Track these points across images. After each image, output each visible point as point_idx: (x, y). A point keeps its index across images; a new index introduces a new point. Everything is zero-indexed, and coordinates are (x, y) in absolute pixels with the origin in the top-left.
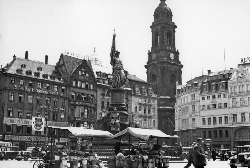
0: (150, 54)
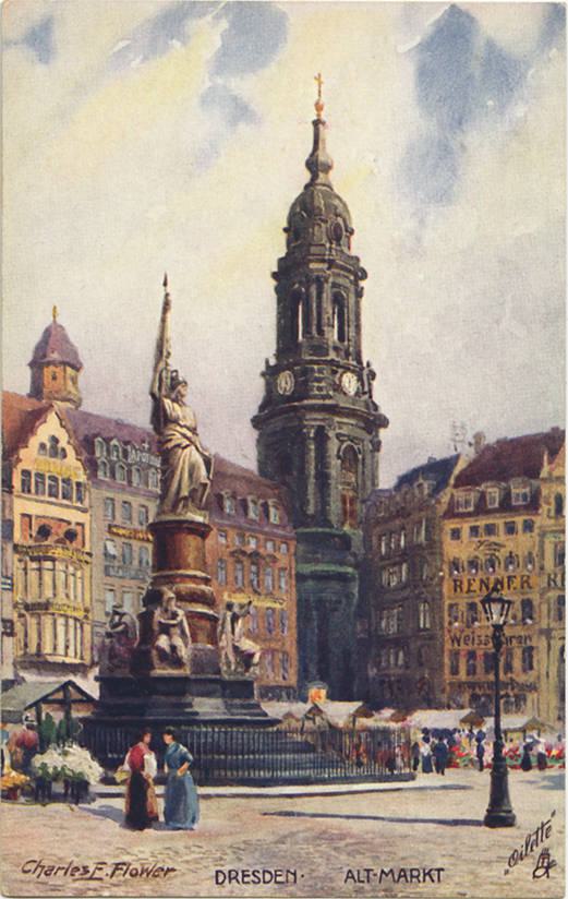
0: (271, 373)
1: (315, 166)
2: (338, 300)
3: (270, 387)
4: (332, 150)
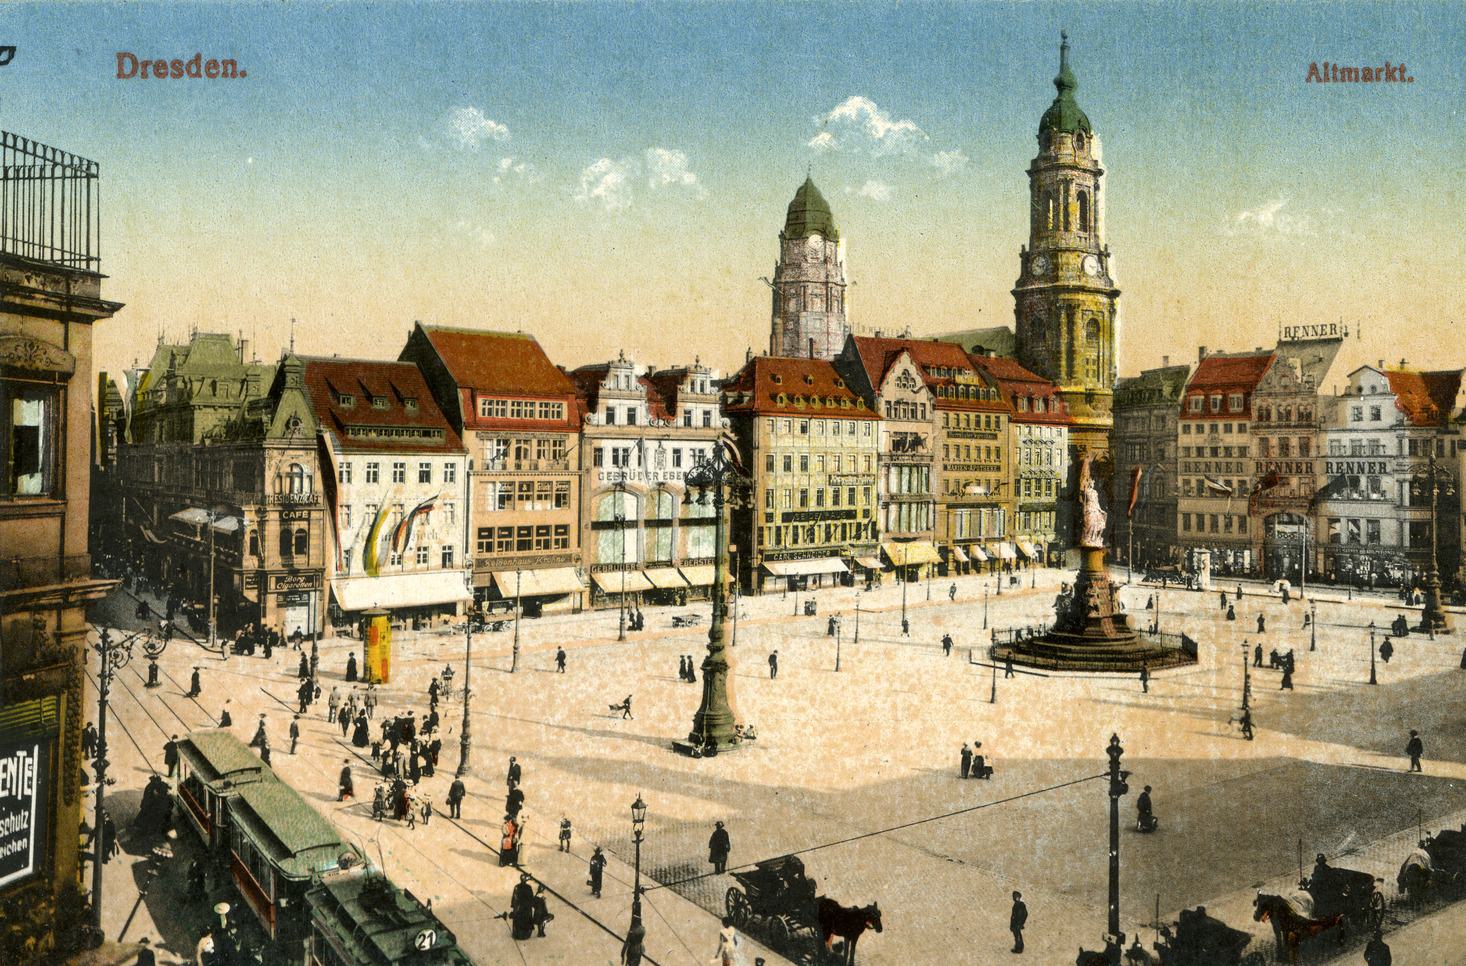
0: (1027, 258)
4: (1077, 72)
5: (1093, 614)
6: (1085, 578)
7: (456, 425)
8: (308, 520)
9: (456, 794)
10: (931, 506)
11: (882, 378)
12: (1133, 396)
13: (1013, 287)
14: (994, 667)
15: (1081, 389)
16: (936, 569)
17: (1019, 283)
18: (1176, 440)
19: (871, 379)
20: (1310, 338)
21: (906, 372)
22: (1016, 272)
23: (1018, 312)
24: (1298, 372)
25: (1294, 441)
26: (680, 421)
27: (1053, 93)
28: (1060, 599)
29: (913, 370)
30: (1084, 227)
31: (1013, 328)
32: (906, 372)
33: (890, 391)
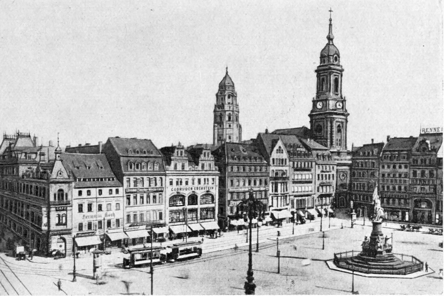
0: (315, 103)
1: (330, 39)
2: (336, 81)
3: (314, 105)
5: (379, 250)
6: (375, 234)
7: (119, 177)
8: (66, 210)
9: (23, 72)
10: (288, 197)
11: (271, 152)
12: (355, 153)
13: (309, 113)
14: (353, 274)
15: (335, 150)
16: (290, 220)
17: (312, 111)
18: (379, 171)
19: (268, 151)
20: (433, 132)
21: (280, 147)
22: (310, 107)
23: (311, 122)
24: (429, 146)
25: (419, 172)
26: (200, 168)
27: (327, 41)
28: (364, 243)
29: (283, 147)
30: (336, 90)
31: (309, 127)
32: (280, 147)
33: (275, 155)
